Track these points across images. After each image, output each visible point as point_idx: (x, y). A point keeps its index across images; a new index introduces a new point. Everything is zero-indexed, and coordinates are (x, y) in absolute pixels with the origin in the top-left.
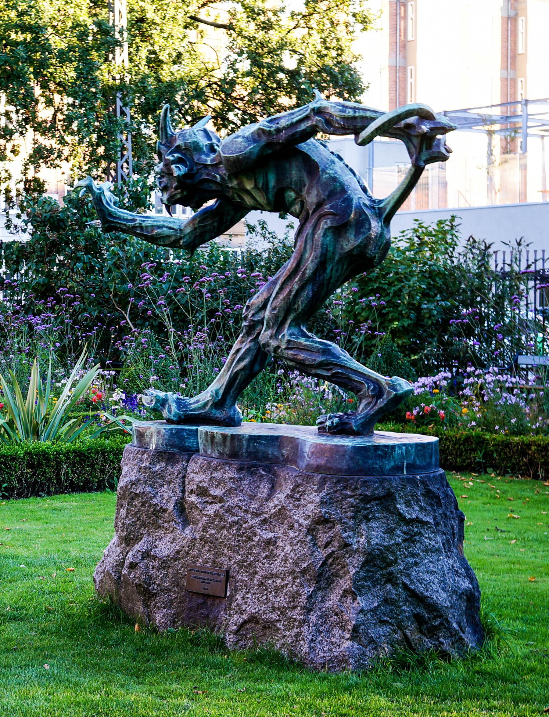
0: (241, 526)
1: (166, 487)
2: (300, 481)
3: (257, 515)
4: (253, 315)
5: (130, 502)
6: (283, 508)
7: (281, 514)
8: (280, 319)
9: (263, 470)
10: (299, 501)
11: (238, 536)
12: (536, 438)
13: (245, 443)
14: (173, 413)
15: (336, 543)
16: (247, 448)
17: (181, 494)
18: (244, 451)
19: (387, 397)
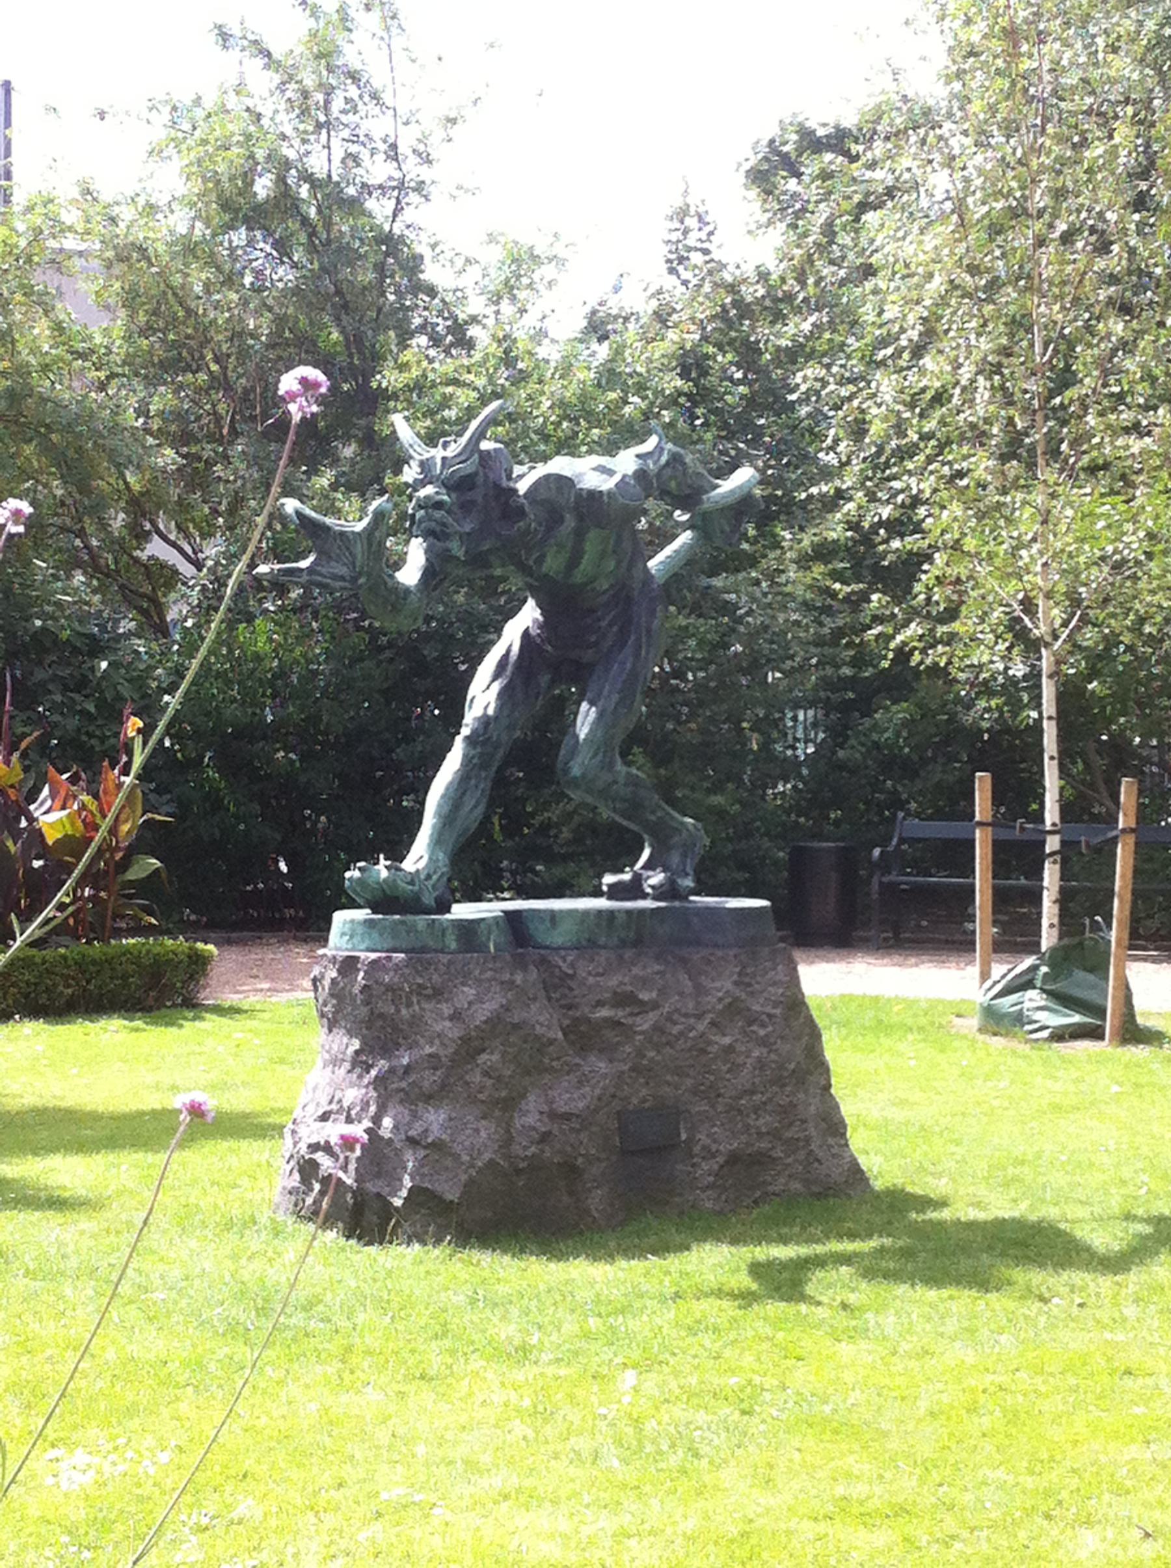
3: (699, 1017)
7: (734, 1009)
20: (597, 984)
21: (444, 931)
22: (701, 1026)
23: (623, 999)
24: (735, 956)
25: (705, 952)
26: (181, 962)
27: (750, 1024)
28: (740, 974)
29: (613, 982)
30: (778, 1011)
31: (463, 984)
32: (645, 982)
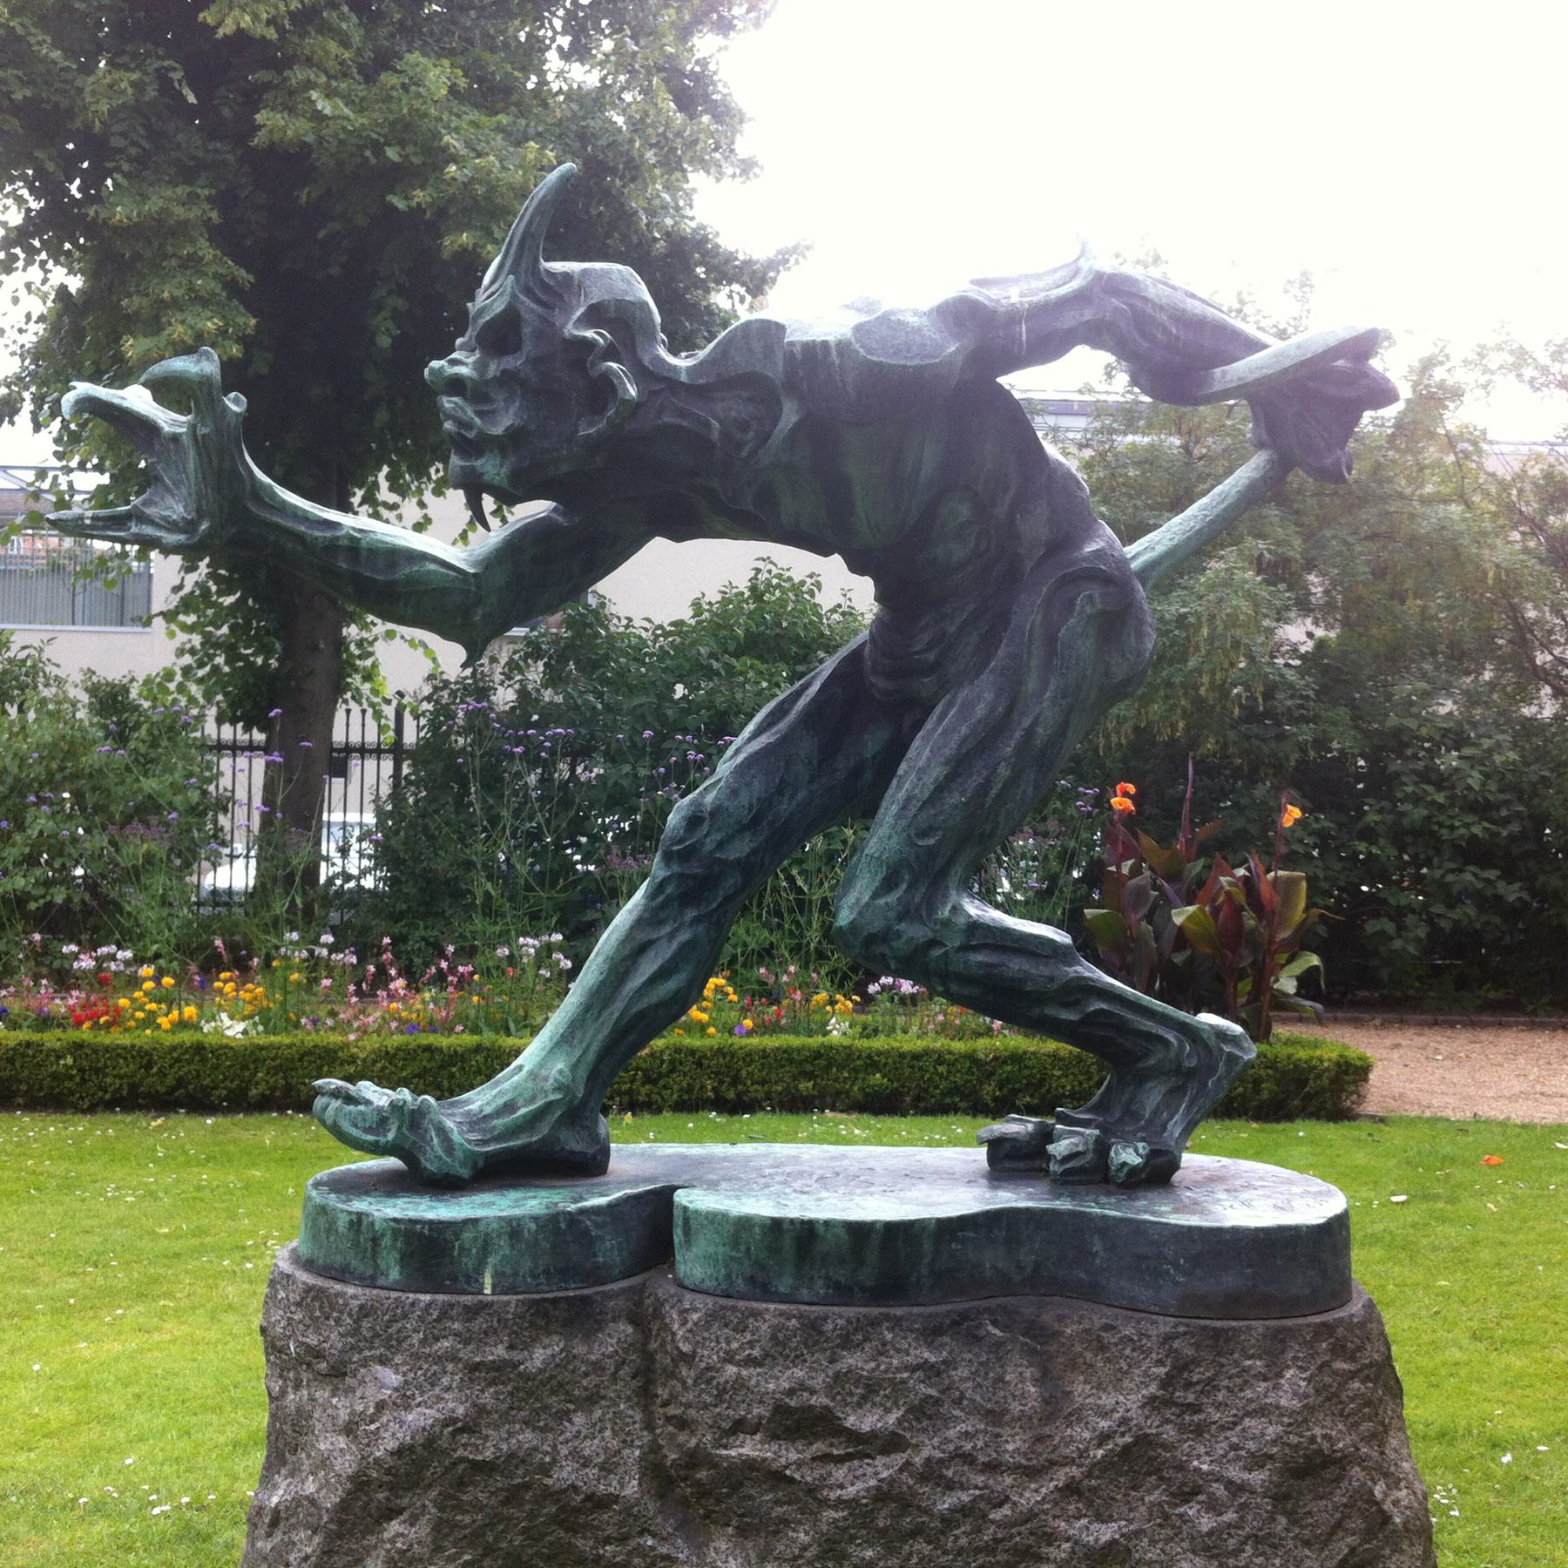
0: (984, 1516)
1: (579, 1419)
2: (1190, 1352)
3: (1032, 1473)
4: (720, 845)
5: (448, 1497)
6: (1143, 1440)
7: (1136, 1460)
8: (940, 862)
9: (995, 1323)
10: (1199, 1411)
11: (978, 1550)
12: (73, 1035)
13: (927, 1246)
14: (459, 1154)
15: (1356, 1523)
16: (933, 1260)
17: (647, 1437)
18: (924, 1270)
19: (1228, 1072)
20: (739, 1384)
21: (375, 1241)
22: (1032, 1496)
23: (793, 1422)
24: (1168, 1338)
25: (1097, 1317)
26: (1327, 1070)
27: (1186, 1496)
28: (1166, 1383)
29: (778, 1382)
30: (1257, 1478)
31: (383, 1361)
32: (869, 1391)
